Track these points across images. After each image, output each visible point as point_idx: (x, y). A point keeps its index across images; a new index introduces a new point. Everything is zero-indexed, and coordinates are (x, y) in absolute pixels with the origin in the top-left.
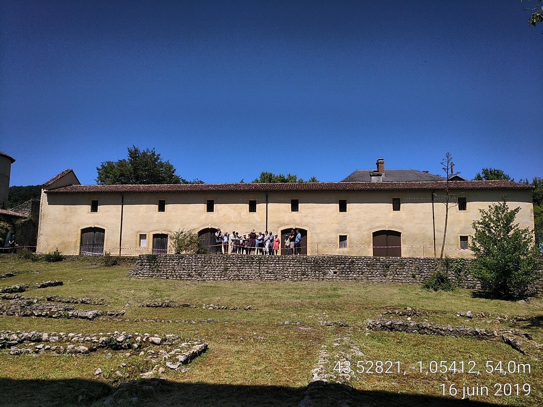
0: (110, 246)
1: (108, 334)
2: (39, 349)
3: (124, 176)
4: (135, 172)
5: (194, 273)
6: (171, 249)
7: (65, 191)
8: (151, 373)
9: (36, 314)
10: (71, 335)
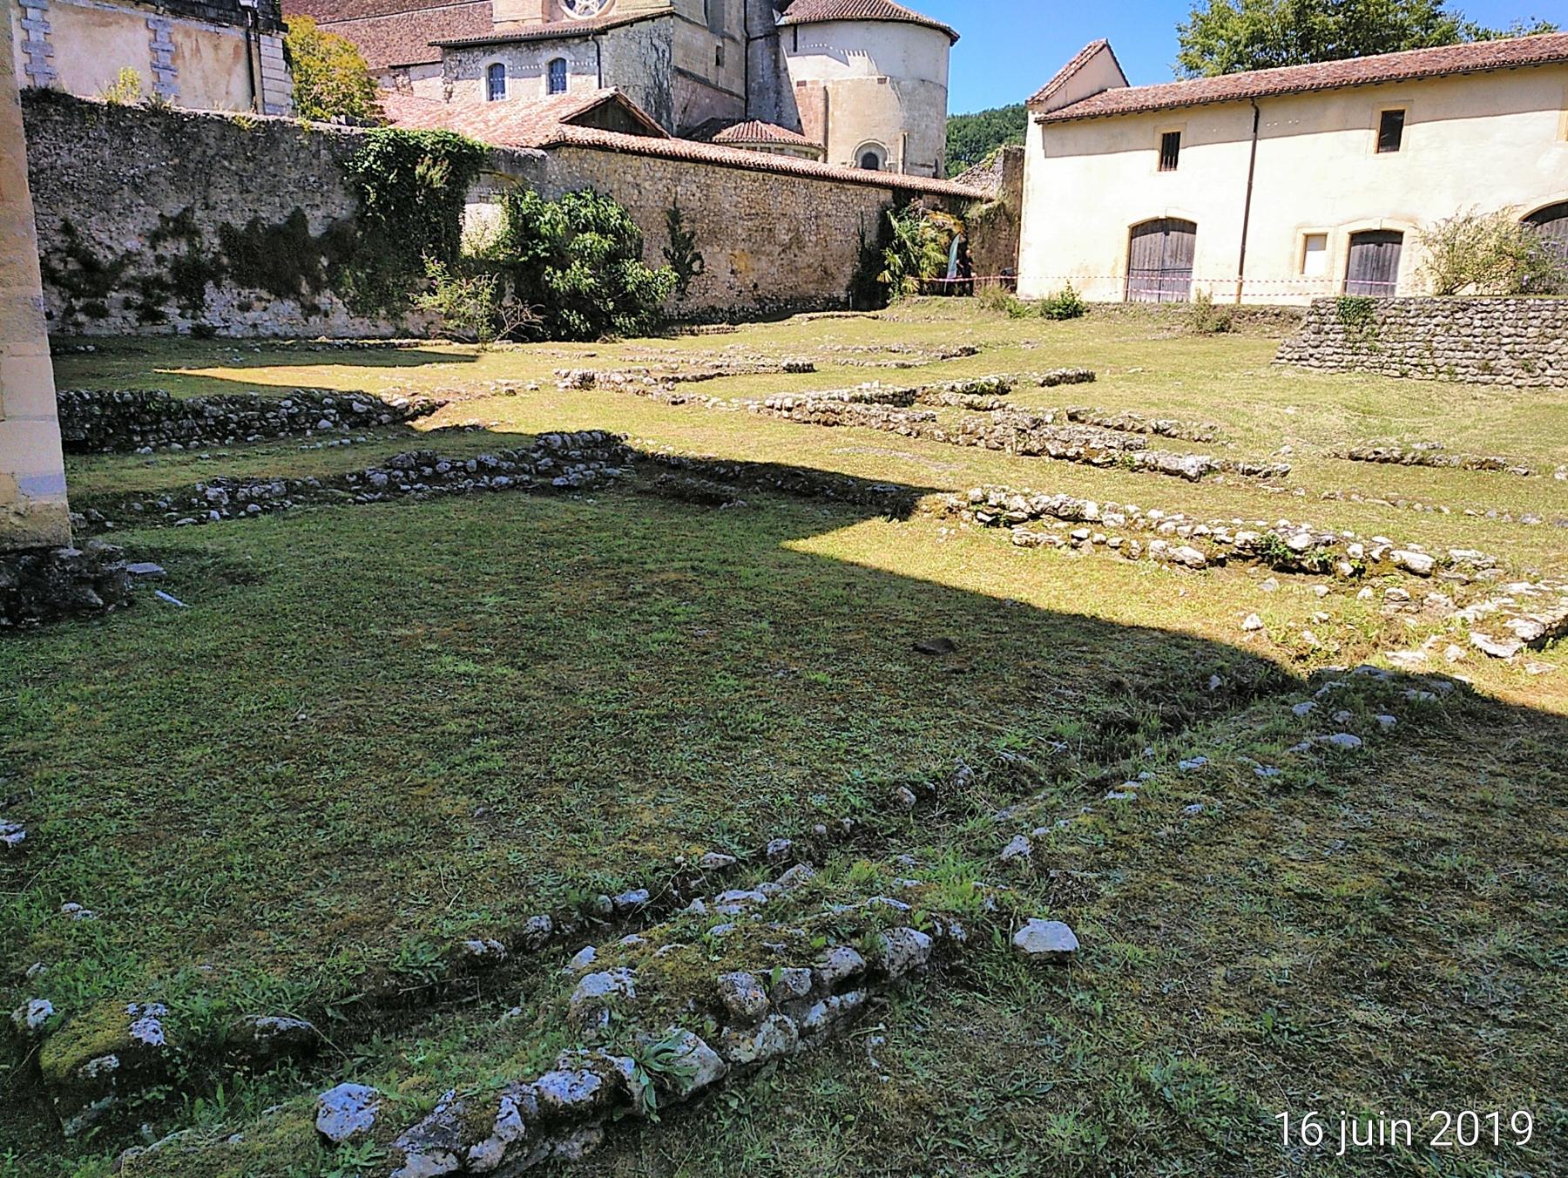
0: (1212, 274)
2: (1080, 539)
3: (1262, 40)
4: (1298, 22)
5: (1505, 360)
6: (1414, 275)
7: (1081, 122)
8: (1420, 654)
9: (1053, 453)
10: (1154, 514)
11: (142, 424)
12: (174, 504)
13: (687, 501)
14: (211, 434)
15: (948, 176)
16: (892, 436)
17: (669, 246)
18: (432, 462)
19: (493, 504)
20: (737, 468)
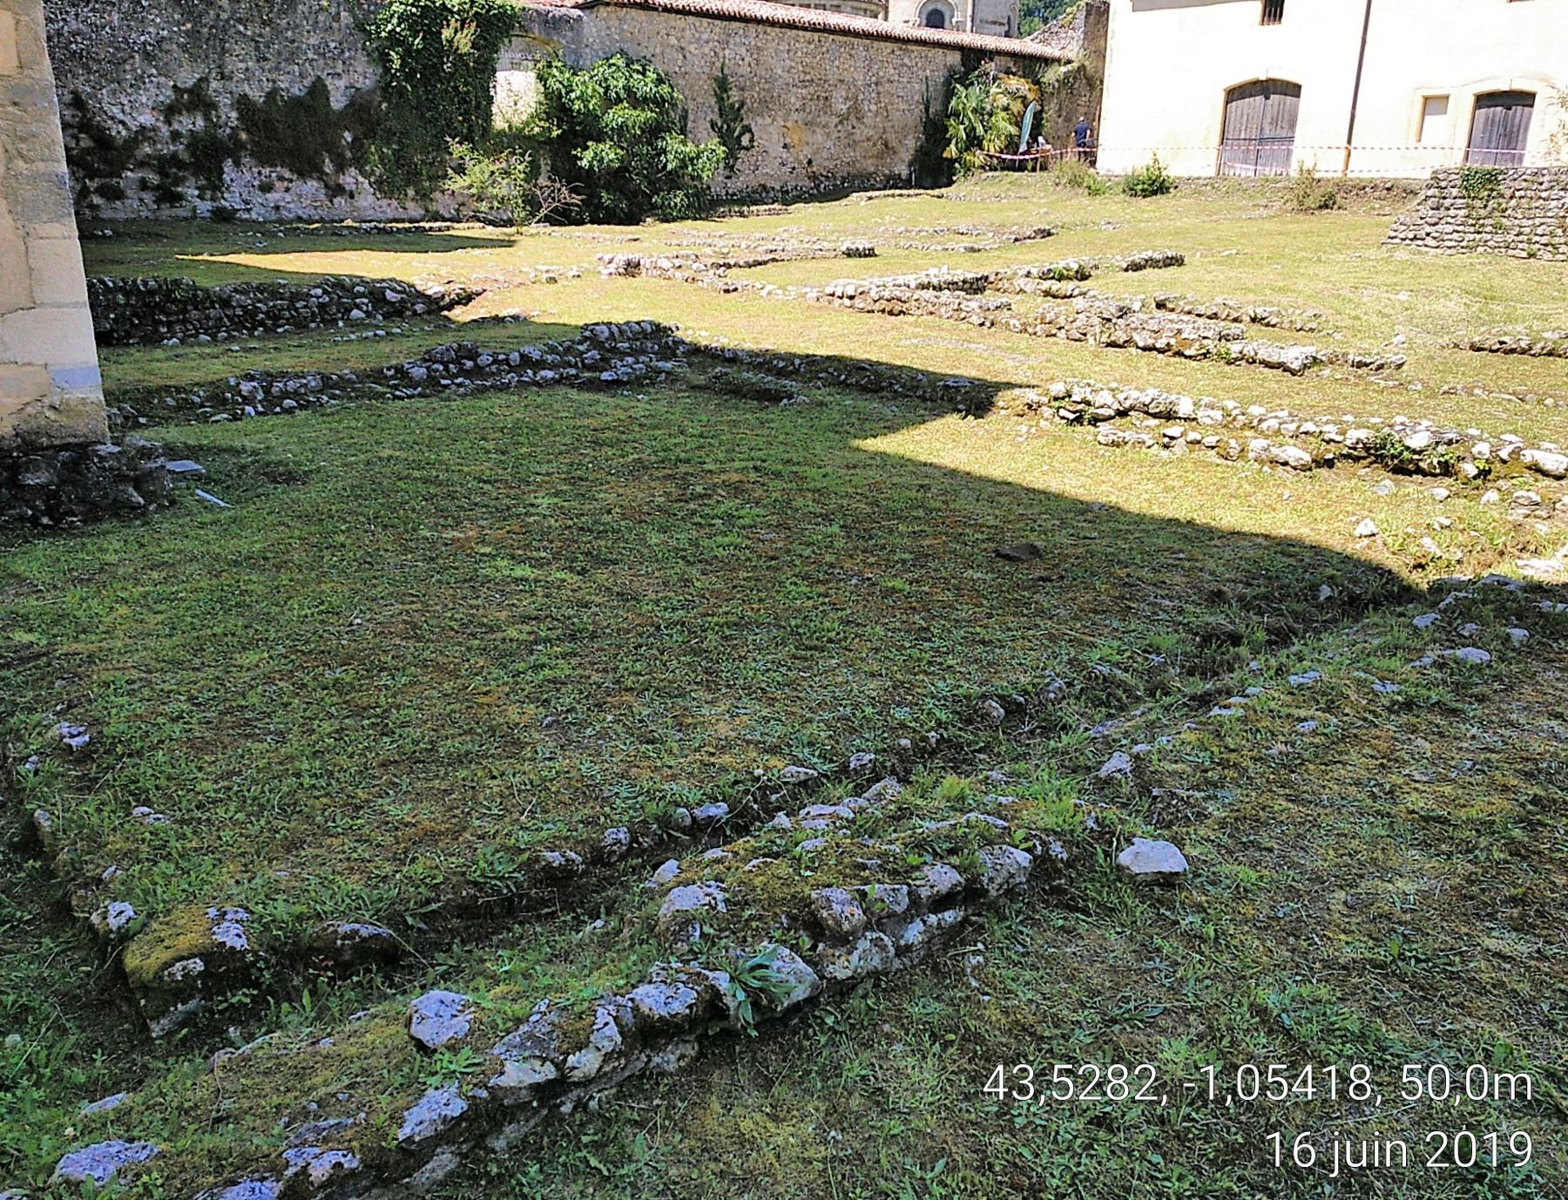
1: (1373, 420)
10: (1256, 410)
11: (168, 315)
12: (208, 399)
13: (744, 396)
14: (238, 324)
15: (1020, 35)
16: (963, 326)
17: (716, 117)
18: (473, 355)
19: (539, 400)
20: (797, 362)
